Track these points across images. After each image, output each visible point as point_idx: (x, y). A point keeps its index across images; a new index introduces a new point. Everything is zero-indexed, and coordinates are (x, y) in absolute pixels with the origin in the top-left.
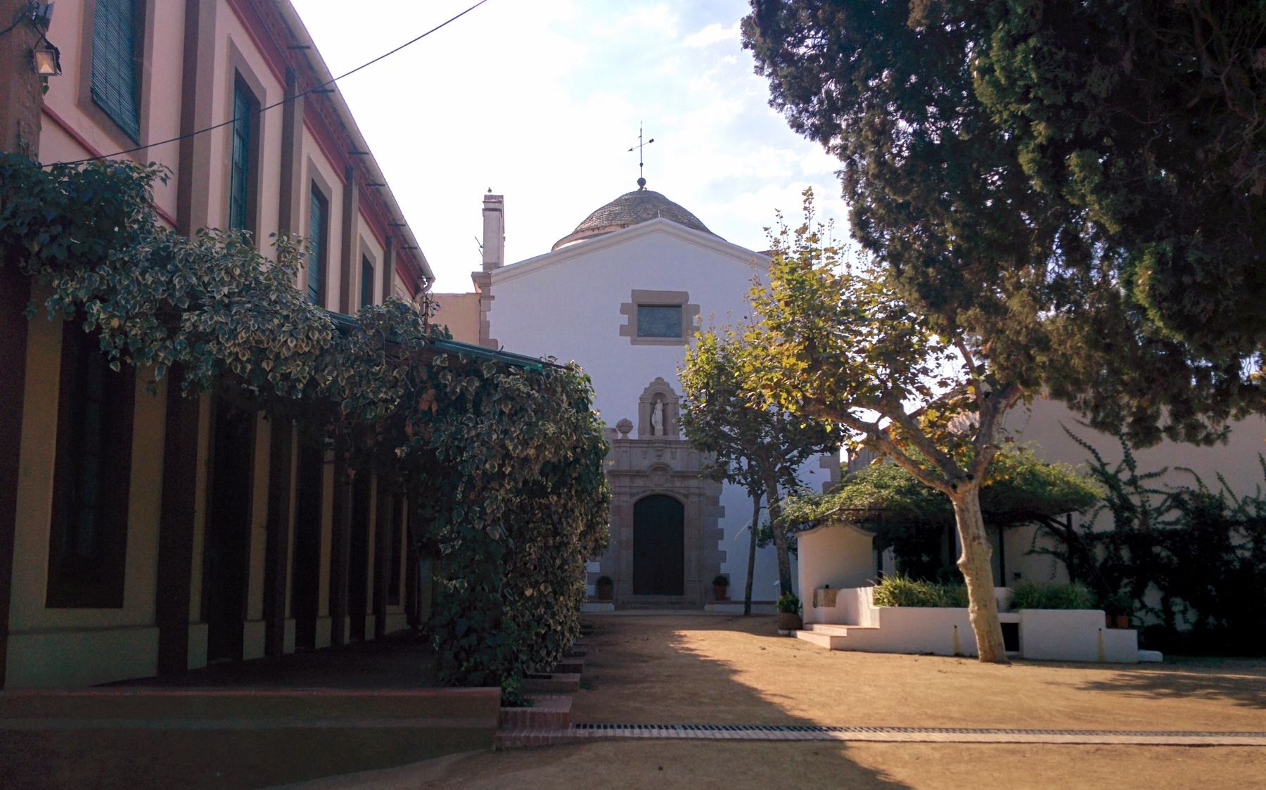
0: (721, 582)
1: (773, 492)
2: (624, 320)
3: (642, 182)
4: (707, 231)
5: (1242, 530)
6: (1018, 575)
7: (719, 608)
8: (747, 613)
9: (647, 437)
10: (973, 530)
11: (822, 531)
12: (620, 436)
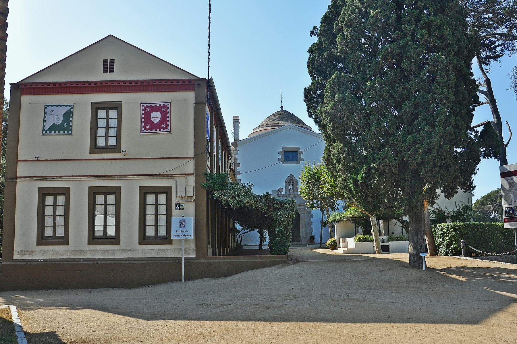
0: (312, 238)
1: (328, 211)
2: (280, 156)
3: (282, 107)
4: (304, 124)
5: (450, 219)
6: (393, 233)
7: (311, 246)
8: (321, 245)
9: (288, 193)
10: (374, 223)
11: (341, 223)
12: (279, 193)
